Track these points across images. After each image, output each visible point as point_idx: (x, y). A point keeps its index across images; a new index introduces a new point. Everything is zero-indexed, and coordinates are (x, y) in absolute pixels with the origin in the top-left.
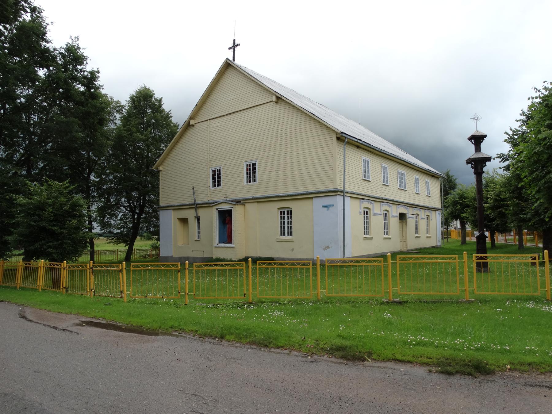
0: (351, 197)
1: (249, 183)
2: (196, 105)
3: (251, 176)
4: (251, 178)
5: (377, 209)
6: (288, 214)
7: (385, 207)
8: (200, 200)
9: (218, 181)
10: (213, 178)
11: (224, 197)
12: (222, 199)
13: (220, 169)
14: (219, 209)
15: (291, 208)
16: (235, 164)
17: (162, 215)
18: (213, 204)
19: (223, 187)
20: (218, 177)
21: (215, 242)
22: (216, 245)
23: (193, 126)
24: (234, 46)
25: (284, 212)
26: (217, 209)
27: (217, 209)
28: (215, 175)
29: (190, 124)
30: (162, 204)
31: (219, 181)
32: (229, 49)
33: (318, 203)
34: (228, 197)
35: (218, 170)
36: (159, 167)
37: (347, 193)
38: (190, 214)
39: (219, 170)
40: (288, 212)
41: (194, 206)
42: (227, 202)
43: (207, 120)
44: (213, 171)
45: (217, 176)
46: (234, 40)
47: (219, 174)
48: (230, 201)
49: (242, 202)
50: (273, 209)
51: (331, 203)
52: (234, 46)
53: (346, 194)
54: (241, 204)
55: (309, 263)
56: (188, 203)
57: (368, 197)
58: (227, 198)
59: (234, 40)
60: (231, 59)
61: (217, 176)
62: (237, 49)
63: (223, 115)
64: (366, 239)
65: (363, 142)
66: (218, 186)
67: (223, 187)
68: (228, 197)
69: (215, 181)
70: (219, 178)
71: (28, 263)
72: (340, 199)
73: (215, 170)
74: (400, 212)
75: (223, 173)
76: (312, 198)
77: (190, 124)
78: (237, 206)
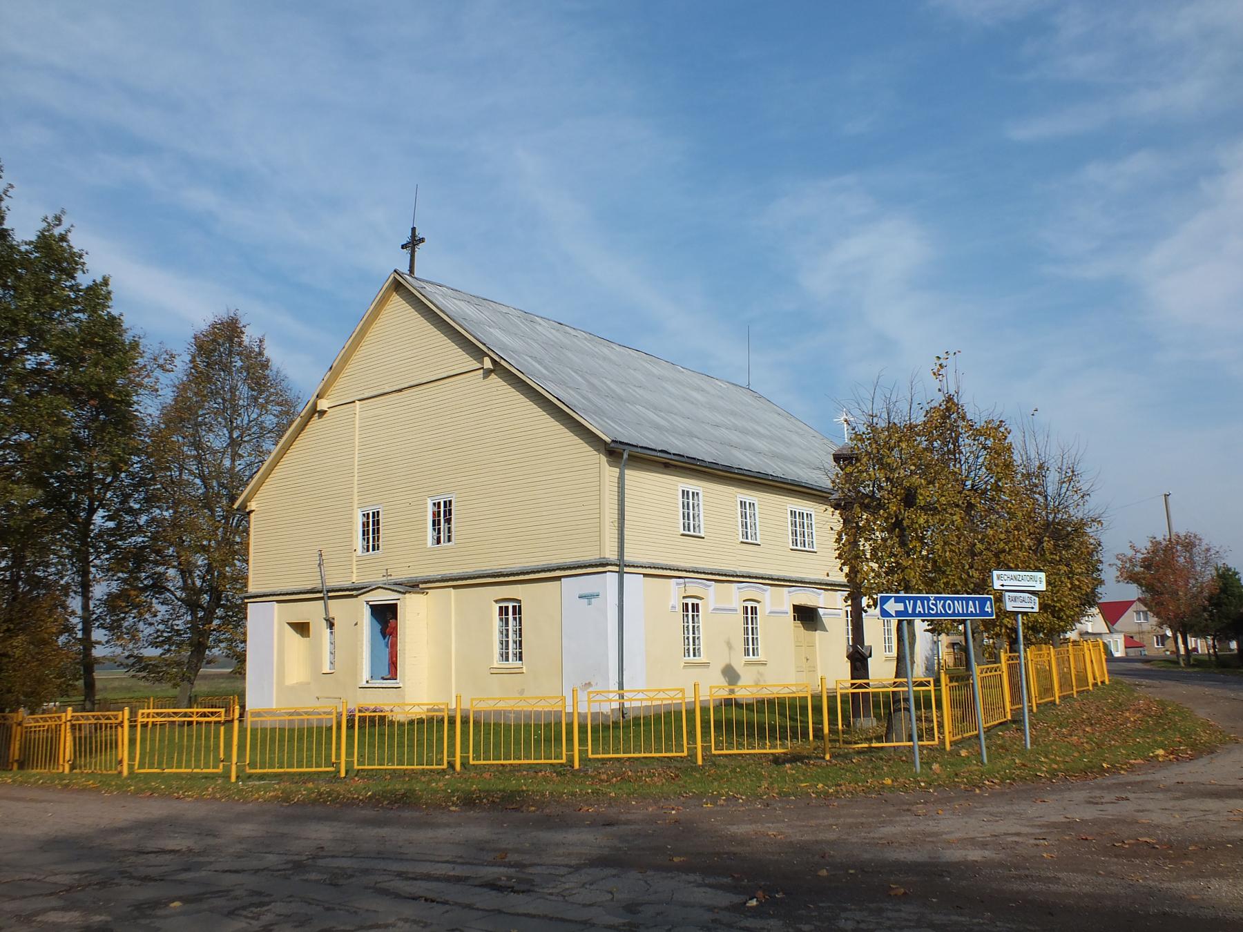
0: (645, 575)
1: (438, 544)
2: (331, 368)
3: (442, 529)
4: (442, 533)
5: (712, 596)
6: (514, 613)
7: (751, 591)
8: (332, 583)
9: (374, 538)
10: (434, 521)
11: (384, 576)
12: (378, 578)
13: (450, 501)
14: (371, 603)
15: (519, 601)
16: (410, 501)
17: (254, 611)
18: (360, 592)
19: (385, 551)
20: (374, 530)
21: (362, 676)
22: (364, 684)
23: (322, 413)
24: (413, 243)
25: (507, 608)
26: (367, 602)
27: (367, 602)
28: (368, 526)
29: (318, 409)
30: (252, 589)
31: (376, 539)
32: (403, 247)
33: (572, 586)
34: (391, 575)
35: (374, 513)
36: (249, 504)
37: (629, 566)
38: (311, 612)
39: (376, 514)
40: (514, 607)
41: (321, 595)
42: (386, 586)
43: (354, 402)
44: (434, 504)
45: (372, 527)
46: (414, 229)
47: (448, 513)
48: (396, 584)
49: (421, 586)
50: (487, 599)
51: (595, 591)
52: (413, 243)
53: (626, 569)
54: (418, 593)
55: (929, 682)
56: (309, 587)
57: (693, 572)
58: (389, 578)
59: (414, 229)
60: (405, 269)
61: (372, 527)
62: (420, 250)
63: (386, 391)
64: (688, 665)
65: (674, 454)
66: (373, 550)
67: (385, 551)
68: (391, 575)
69: (368, 538)
70: (376, 531)
71: (41, 718)
72: (611, 579)
73: (439, 503)
74: (796, 603)
75: (385, 521)
76: (558, 578)
77: (318, 409)
78: (407, 595)
